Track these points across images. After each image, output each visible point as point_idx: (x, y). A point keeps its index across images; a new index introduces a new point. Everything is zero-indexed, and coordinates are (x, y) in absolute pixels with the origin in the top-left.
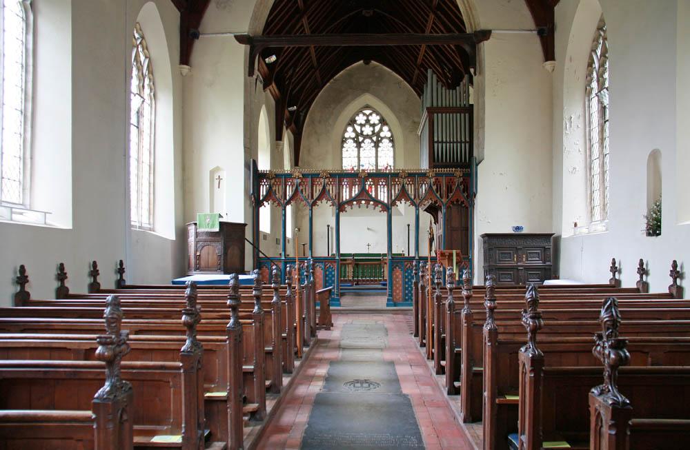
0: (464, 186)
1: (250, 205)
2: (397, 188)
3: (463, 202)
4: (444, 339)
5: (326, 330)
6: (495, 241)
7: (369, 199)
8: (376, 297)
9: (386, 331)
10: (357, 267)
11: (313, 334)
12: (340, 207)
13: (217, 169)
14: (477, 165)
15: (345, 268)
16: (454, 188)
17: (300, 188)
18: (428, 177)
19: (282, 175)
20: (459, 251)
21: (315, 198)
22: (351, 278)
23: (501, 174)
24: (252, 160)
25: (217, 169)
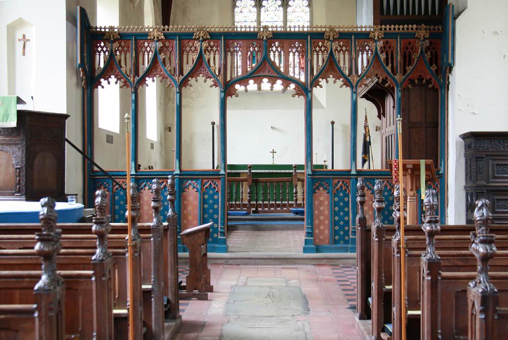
0: (431, 53)
1: (78, 84)
2: (320, 56)
3: (429, 82)
4: (389, 293)
5: (199, 299)
6: (486, 144)
7: (276, 74)
8: (284, 232)
9: (305, 301)
10: (256, 186)
11: (171, 312)
12: (228, 89)
13: (20, 23)
14: (455, 18)
15: (238, 187)
16: (415, 57)
17: (162, 56)
18: (373, 39)
19: (130, 35)
20: (430, 161)
21: (185, 73)
22: (246, 202)
23: (496, 33)
24: (79, 7)
25: (20, 23)
